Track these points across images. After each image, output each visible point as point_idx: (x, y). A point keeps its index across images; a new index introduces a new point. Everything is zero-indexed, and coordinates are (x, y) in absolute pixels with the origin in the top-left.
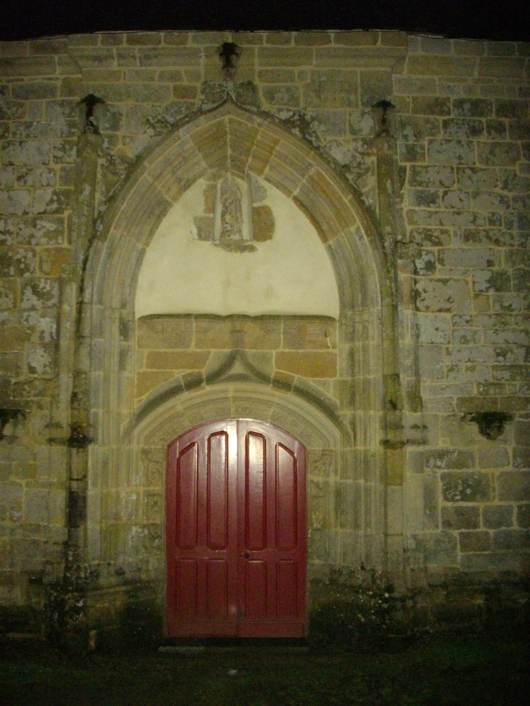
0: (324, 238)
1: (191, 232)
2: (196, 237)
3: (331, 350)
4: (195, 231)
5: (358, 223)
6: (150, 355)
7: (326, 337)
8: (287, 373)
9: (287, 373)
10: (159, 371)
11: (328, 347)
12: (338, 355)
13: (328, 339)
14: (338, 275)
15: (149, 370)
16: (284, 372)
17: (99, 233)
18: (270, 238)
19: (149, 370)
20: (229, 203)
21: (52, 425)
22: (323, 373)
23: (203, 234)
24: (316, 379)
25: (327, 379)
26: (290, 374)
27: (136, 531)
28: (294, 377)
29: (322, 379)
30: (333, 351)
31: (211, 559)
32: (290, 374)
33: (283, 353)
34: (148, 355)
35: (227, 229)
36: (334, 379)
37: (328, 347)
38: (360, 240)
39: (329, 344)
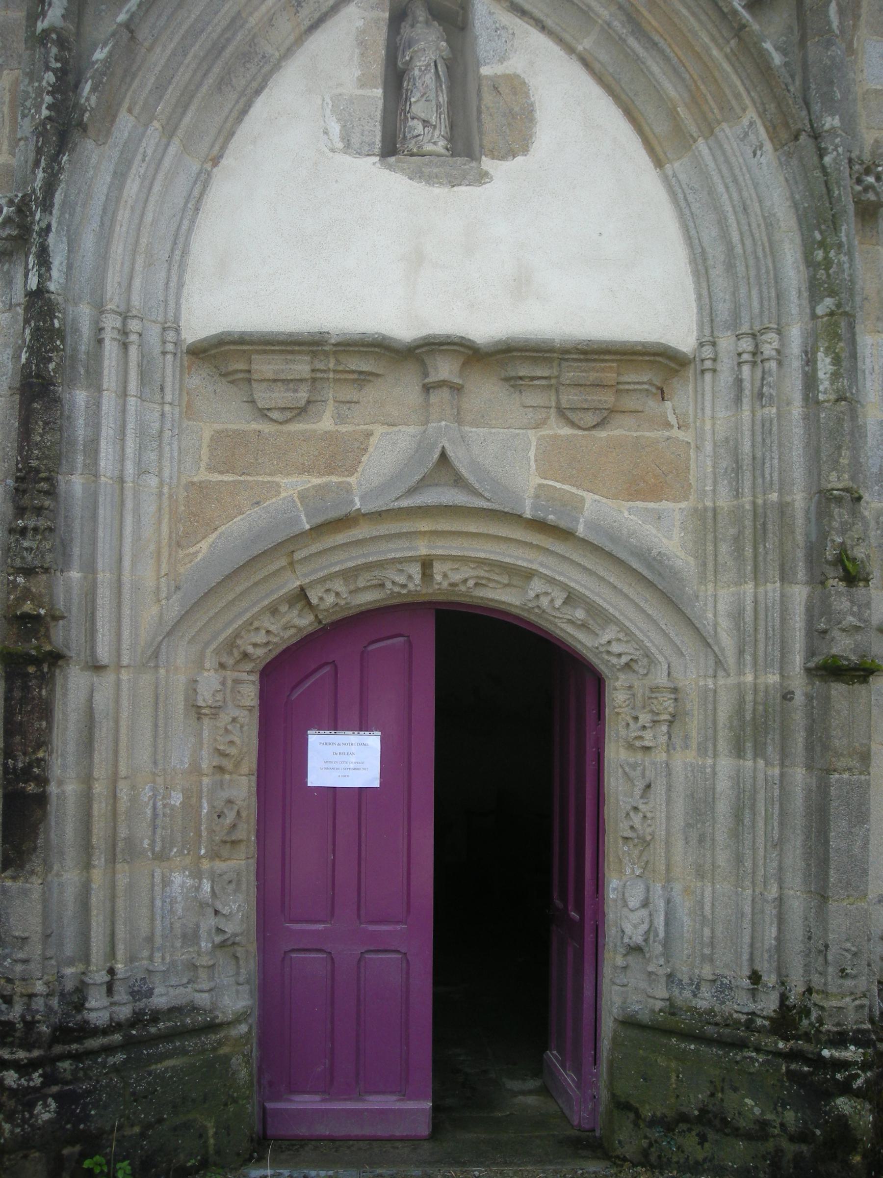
0: (659, 163)
1: (326, 133)
2: (340, 145)
3: (675, 433)
4: (335, 129)
5: (751, 114)
6: (218, 438)
7: (663, 399)
8: (566, 487)
9: (566, 487)
10: (241, 478)
11: (668, 425)
12: (693, 445)
13: (668, 404)
14: (691, 239)
15: (217, 477)
16: (558, 485)
17: (87, 115)
18: (525, 149)
19: (217, 477)
20: (420, 70)
21: (712, 943)
22: (654, 492)
23: (355, 140)
24: (639, 504)
25: (665, 504)
26: (574, 490)
27: (182, 886)
28: (582, 500)
29: (652, 505)
30: (681, 435)
31: (410, 104)
32: (574, 490)
33: (556, 437)
34: (212, 439)
35: (416, 132)
36: (683, 505)
37: (668, 425)
38: (755, 154)
39: (672, 419)
